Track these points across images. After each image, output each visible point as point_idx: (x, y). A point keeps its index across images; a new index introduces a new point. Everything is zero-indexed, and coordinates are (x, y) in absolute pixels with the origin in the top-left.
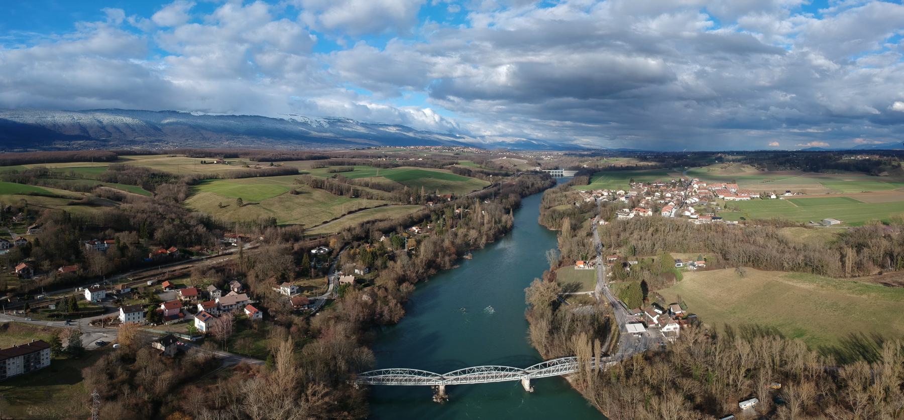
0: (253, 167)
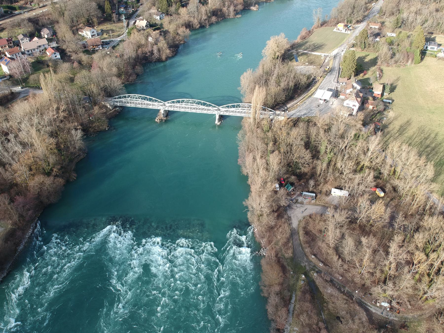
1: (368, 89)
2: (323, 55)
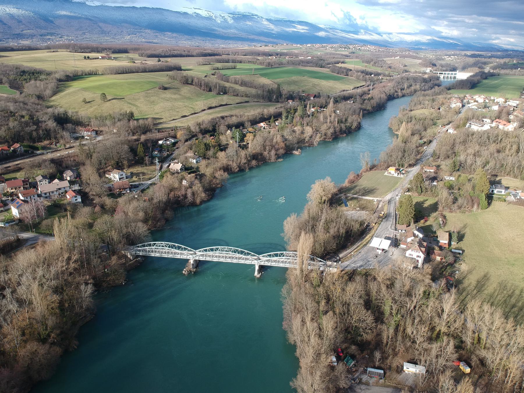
0: (140, 61)
1: (432, 237)
2: (375, 199)
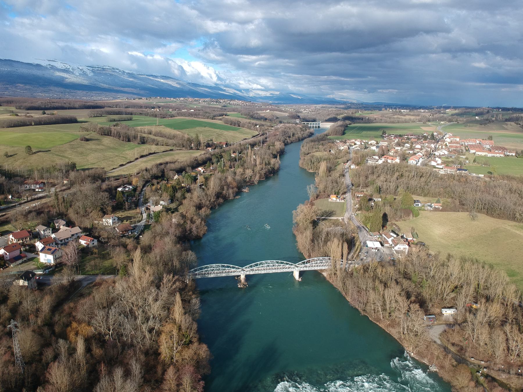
0: (22, 115)
